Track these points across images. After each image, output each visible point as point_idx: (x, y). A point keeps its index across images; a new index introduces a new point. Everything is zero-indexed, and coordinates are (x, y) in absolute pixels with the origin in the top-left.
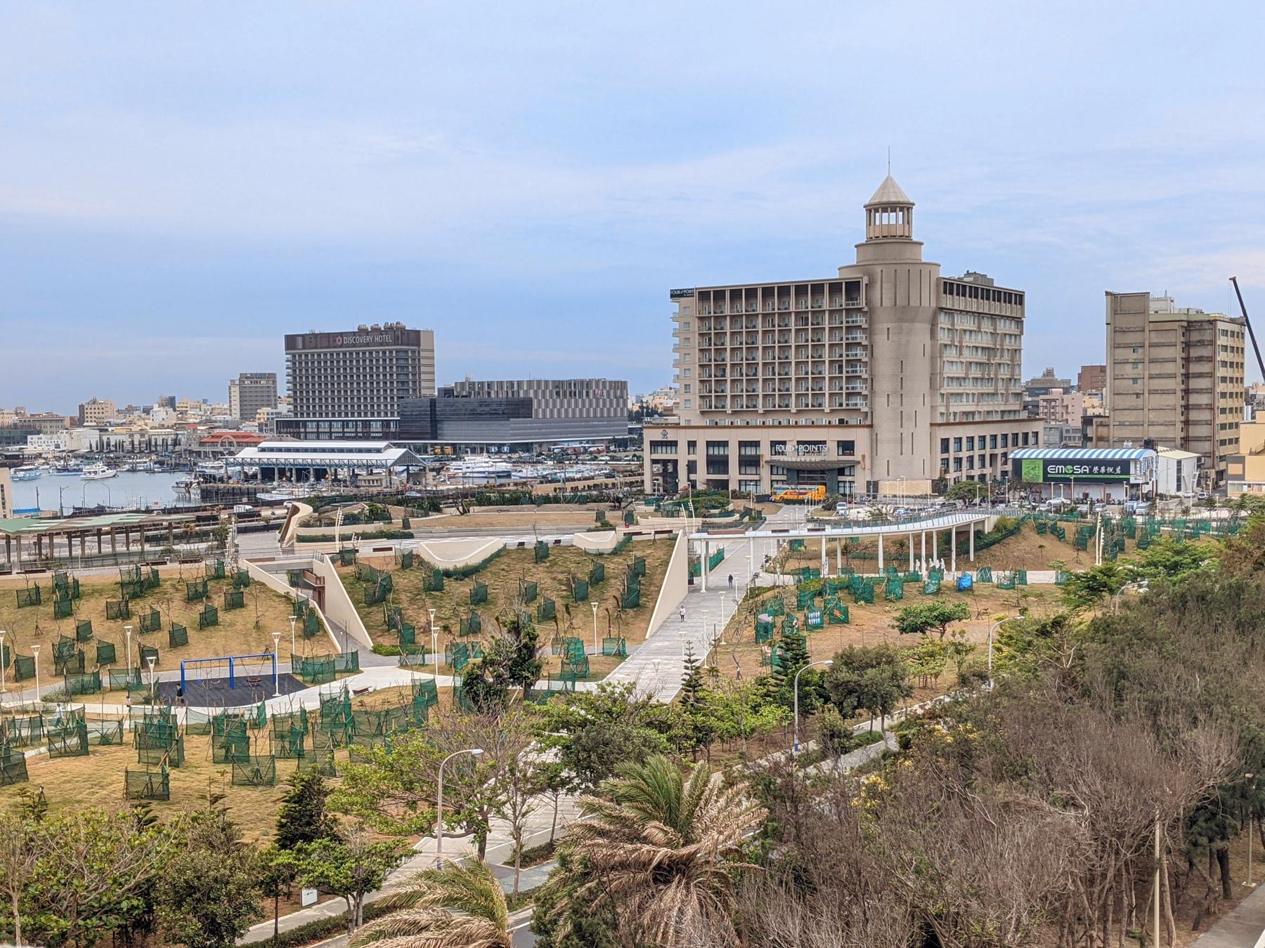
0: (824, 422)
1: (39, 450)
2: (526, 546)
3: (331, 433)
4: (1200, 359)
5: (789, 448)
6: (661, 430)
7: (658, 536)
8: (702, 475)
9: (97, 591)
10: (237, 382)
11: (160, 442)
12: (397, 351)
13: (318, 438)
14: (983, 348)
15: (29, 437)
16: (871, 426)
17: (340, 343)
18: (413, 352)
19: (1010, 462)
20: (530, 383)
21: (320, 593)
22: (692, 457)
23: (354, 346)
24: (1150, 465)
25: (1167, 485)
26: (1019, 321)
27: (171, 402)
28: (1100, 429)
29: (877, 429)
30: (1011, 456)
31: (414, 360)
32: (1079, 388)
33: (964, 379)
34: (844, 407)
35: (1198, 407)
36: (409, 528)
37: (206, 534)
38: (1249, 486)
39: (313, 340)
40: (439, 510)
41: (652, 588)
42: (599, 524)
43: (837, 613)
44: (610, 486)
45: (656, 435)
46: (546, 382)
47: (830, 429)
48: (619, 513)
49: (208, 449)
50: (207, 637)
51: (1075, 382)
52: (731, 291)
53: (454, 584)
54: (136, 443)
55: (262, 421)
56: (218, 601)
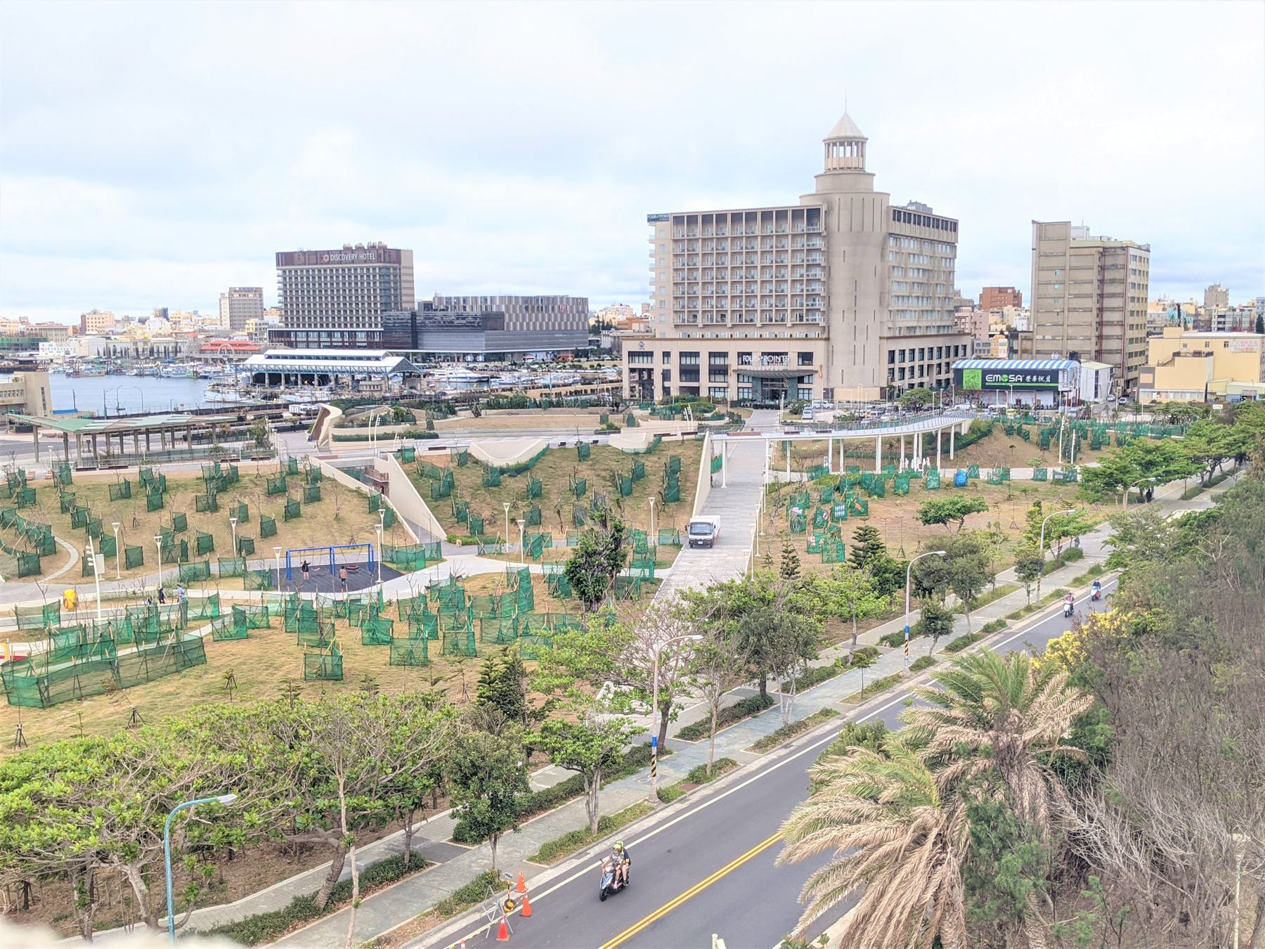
0: (727, 334)
1: (50, 356)
2: (567, 446)
3: (319, 342)
4: (1113, 281)
5: (755, 358)
6: (638, 342)
7: (686, 437)
8: (675, 384)
9: (181, 486)
10: (227, 295)
11: (162, 350)
12: (380, 269)
13: (308, 347)
14: (923, 270)
15: (41, 344)
16: (828, 339)
17: (327, 261)
18: (395, 269)
19: (951, 371)
20: (501, 298)
21: (384, 487)
22: (666, 367)
23: (341, 262)
24: (1075, 378)
25: (1087, 394)
26: (952, 245)
27: (164, 314)
28: (1024, 342)
29: (832, 341)
30: (954, 366)
31: (395, 276)
32: (980, 307)
33: (908, 297)
34: (805, 322)
35: (1111, 324)
36: (433, 429)
37: (242, 433)
38: (1159, 393)
39: (302, 257)
40: (454, 413)
41: (688, 484)
42: (604, 426)
43: (857, 506)
44: (589, 392)
45: (634, 346)
46: (517, 298)
47: (792, 342)
48: (621, 416)
49: (209, 356)
50: (293, 528)
51: (977, 302)
52: (733, 215)
53: (511, 480)
54: (140, 350)
55: (251, 331)
56: (298, 495)
